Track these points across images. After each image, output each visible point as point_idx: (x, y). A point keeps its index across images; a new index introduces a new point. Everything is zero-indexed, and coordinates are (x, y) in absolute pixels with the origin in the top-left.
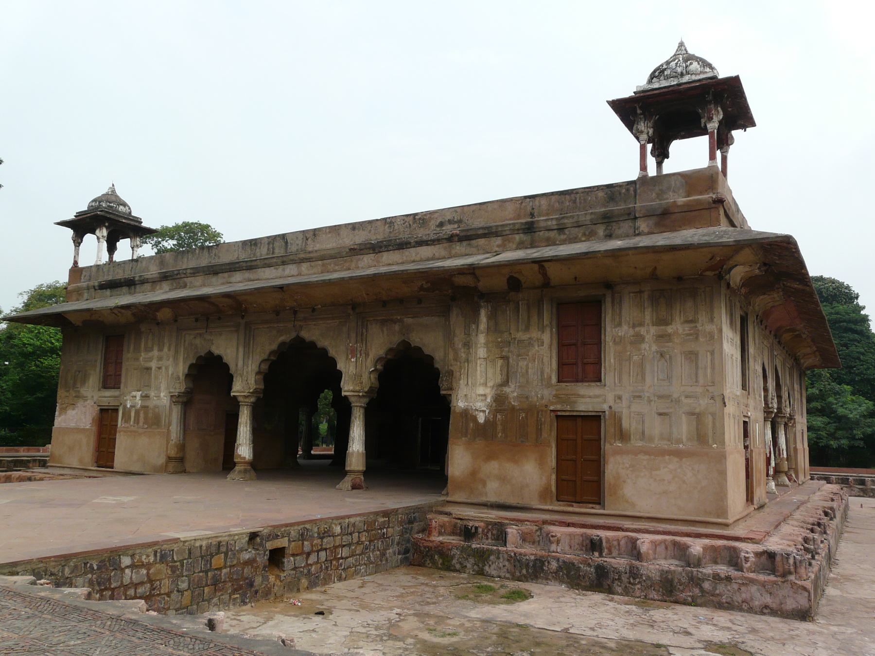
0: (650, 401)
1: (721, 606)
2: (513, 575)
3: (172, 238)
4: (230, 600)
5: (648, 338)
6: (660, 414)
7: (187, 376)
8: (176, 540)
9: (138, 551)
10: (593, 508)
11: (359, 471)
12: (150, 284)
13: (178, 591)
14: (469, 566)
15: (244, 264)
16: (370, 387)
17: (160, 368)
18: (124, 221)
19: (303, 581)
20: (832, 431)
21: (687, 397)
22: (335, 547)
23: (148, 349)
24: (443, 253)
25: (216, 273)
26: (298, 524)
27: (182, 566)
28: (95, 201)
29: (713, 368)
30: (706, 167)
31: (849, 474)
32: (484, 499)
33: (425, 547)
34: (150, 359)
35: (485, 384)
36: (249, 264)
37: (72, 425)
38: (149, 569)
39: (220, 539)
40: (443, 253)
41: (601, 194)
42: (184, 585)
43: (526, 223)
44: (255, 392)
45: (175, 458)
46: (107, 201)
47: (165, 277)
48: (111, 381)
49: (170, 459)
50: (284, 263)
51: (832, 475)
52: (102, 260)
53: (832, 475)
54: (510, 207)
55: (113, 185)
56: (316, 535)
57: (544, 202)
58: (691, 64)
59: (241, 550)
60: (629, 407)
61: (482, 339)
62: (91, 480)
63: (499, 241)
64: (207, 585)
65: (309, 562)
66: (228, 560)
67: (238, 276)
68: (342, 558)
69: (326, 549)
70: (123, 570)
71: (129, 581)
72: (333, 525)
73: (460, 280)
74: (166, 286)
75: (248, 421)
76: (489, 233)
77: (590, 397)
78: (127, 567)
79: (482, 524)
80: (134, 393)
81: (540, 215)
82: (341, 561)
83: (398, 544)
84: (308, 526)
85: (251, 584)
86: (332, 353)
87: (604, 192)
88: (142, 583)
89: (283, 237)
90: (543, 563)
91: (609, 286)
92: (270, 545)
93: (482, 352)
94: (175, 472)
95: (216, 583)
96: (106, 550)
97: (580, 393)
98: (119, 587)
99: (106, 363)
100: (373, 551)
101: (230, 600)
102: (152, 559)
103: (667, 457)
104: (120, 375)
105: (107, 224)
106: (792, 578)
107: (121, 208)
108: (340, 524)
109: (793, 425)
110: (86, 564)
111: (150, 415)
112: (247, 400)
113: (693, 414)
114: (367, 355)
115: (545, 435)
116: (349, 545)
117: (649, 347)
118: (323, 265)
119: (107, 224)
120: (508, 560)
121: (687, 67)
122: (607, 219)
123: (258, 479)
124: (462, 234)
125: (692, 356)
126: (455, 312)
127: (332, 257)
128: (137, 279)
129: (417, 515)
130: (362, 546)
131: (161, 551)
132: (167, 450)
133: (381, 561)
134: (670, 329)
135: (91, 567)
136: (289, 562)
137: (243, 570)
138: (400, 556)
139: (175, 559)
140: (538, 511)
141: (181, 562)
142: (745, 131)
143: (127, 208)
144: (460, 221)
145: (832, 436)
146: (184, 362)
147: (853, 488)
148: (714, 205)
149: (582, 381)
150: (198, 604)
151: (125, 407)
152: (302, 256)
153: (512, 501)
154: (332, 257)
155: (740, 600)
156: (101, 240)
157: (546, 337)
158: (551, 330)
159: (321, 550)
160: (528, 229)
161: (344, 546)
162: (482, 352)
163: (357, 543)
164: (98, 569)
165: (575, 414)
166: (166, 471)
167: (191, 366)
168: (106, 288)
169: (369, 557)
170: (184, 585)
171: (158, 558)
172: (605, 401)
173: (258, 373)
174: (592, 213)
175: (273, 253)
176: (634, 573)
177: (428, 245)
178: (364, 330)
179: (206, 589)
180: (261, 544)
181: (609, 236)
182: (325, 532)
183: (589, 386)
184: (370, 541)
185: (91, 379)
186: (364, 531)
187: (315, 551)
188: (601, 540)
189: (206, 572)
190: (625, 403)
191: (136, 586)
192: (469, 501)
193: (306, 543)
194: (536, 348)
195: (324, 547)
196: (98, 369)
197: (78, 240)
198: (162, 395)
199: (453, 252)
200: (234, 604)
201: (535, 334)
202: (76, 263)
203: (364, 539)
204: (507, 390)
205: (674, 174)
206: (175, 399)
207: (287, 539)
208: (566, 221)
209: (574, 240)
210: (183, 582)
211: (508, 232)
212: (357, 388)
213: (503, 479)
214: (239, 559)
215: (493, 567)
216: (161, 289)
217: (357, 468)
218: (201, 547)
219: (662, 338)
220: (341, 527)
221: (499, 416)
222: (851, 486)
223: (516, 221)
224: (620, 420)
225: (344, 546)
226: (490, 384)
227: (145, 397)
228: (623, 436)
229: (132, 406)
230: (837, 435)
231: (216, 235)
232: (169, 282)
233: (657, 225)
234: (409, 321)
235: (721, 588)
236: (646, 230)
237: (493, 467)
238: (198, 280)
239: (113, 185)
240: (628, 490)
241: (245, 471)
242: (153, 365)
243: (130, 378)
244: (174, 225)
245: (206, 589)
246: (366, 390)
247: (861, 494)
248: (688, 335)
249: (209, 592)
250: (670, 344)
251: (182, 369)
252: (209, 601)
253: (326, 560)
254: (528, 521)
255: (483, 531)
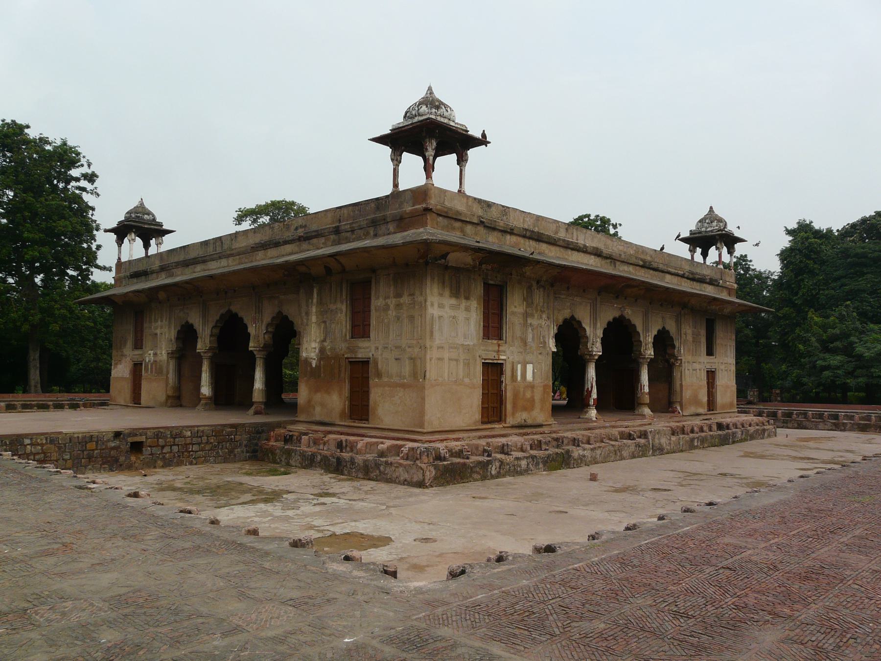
0: (391, 350)
1: (389, 481)
2: (301, 464)
3: (267, 215)
4: (101, 468)
5: (392, 306)
6: (396, 359)
7: (177, 339)
8: (60, 433)
9: (35, 437)
10: (364, 423)
11: (260, 402)
12: (155, 274)
13: (63, 459)
14: (283, 460)
15: (200, 259)
16: (264, 344)
17: (162, 334)
18: (146, 226)
19: (159, 462)
20: (850, 369)
21: (409, 347)
22: (186, 444)
23: (156, 321)
24: (296, 249)
25: (188, 266)
26: (154, 428)
27: (65, 446)
28: (127, 213)
29: (421, 327)
30: (388, 193)
31: (793, 409)
32: (313, 419)
33: (265, 448)
34: (156, 328)
35: (315, 341)
36: (203, 259)
37: (120, 375)
38: (42, 447)
39: (92, 434)
40: (296, 249)
41: (373, 205)
42: (67, 457)
43: (335, 227)
44: (210, 349)
45: (173, 397)
46: (136, 213)
47: (163, 269)
48: (138, 345)
49: (168, 397)
50: (220, 258)
51: (840, 412)
52: (133, 256)
53: (840, 412)
54: (330, 215)
55: (142, 199)
56: (169, 436)
57: (345, 211)
58: (421, 107)
59: (108, 441)
60: (382, 355)
61: (314, 309)
62: (105, 411)
63: (322, 240)
64: (83, 458)
65: (164, 452)
66: (99, 446)
67: (199, 268)
68: (192, 451)
69: (178, 445)
70: (25, 446)
71: (30, 452)
72: (184, 431)
73: (303, 269)
74: (163, 275)
75: (208, 370)
76: (318, 234)
77: (364, 348)
78: (28, 444)
79: (296, 434)
80: (150, 352)
81: (343, 221)
82: (191, 453)
83: (246, 446)
84: (162, 430)
85: (117, 460)
86: (246, 321)
87: (87, 270)
88: (38, 453)
89: (220, 238)
90: (314, 456)
91: (374, 271)
92: (130, 440)
93: (314, 319)
94: (172, 406)
95: (90, 458)
96: (14, 435)
97: (360, 346)
98: (24, 454)
99: (136, 332)
100: (222, 449)
101: (101, 468)
102: (44, 442)
103: (398, 388)
104: (143, 340)
105: (134, 230)
106: (418, 462)
107: (146, 217)
108: (190, 430)
109: (680, 364)
110: (2, 441)
111: (158, 367)
112: (206, 355)
113: (412, 359)
114: (262, 321)
115: (342, 375)
116: (199, 444)
117: (392, 313)
118: (240, 258)
119: (134, 230)
120: (300, 456)
121: (418, 110)
122: (374, 223)
123: (217, 410)
124: (305, 236)
125: (411, 318)
126: (301, 291)
127: (244, 253)
128: (148, 270)
129: (265, 428)
130: (211, 445)
131: (50, 438)
132: (166, 391)
133: (230, 455)
134: (402, 300)
135: (5, 442)
136: (147, 451)
137: (110, 452)
138: (248, 454)
139: (60, 442)
140: (444, 433)
141: (65, 445)
142: (486, 146)
143: (151, 216)
144: (305, 226)
145: (851, 374)
146: (175, 329)
147: (827, 423)
148: (424, 213)
149: (363, 337)
150: (77, 468)
151: (146, 361)
152: (229, 252)
153: (327, 420)
154: (244, 253)
155: (395, 477)
156: (131, 242)
157: (344, 307)
158: (347, 302)
159: (174, 445)
160: (336, 231)
161: (194, 444)
162: (314, 319)
163: (207, 443)
164: (9, 444)
165: (357, 360)
166: (166, 406)
167: (179, 332)
168: (134, 278)
169: (218, 453)
170: (67, 457)
171: (48, 441)
172: (370, 351)
173: (211, 336)
174: (367, 219)
175: (216, 250)
176: (352, 461)
177: (289, 244)
178: (260, 304)
179: (83, 460)
180: (124, 438)
181: (376, 236)
182: (176, 435)
183: (364, 341)
184: (219, 443)
185: (128, 343)
186: (212, 436)
187: (168, 446)
188: (341, 441)
189: (83, 451)
190: (380, 352)
191: (35, 454)
192: (306, 420)
193: (160, 440)
194: (339, 315)
195: (176, 443)
196: (131, 335)
197: (120, 241)
198: (163, 352)
199: (301, 249)
200: (104, 470)
201: (339, 305)
202: (119, 258)
203: (212, 441)
204: (325, 344)
205: (407, 190)
206: (171, 355)
207: (144, 437)
208: (354, 225)
209: (359, 239)
210: (66, 455)
211: (327, 234)
212: (256, 345)
213: (323, 405)
214: (106, 446)
215: (294, 460)
216: (161, 277)
217: (258, 400)
218: (78, 437)
219: (399, 306)
220: (191, 433)
221: (322, 363)
222: (824, 421)
223: (330, 226)
224: (377, 364)
225: (194, 444)
226: (318, 341)
227: (155, 354)
228: (379, 375)
229: (149, 361)
230: (856, 374)
231: (302, 210)
232: (165, 272)
233: (398, 226)
234: (282, 297)
235: (388, 470)
236: (393, 231)
237: (318, 397)
238: (178, 271)
239: (142, 199)
240: (380, 411)
241: (206, 404)
242: (158, 331)
243: (147, 342)
244: (264, 204)
245: (83, 460)
246: (262, 346)
247: (834, 428)
248: (410, 304)
249: (85, 462)
250: (402, 311)
251: (173, 334)
252: (86, 467)
253: (178, 452)
254: (319, 431)
255: (297, 438)
